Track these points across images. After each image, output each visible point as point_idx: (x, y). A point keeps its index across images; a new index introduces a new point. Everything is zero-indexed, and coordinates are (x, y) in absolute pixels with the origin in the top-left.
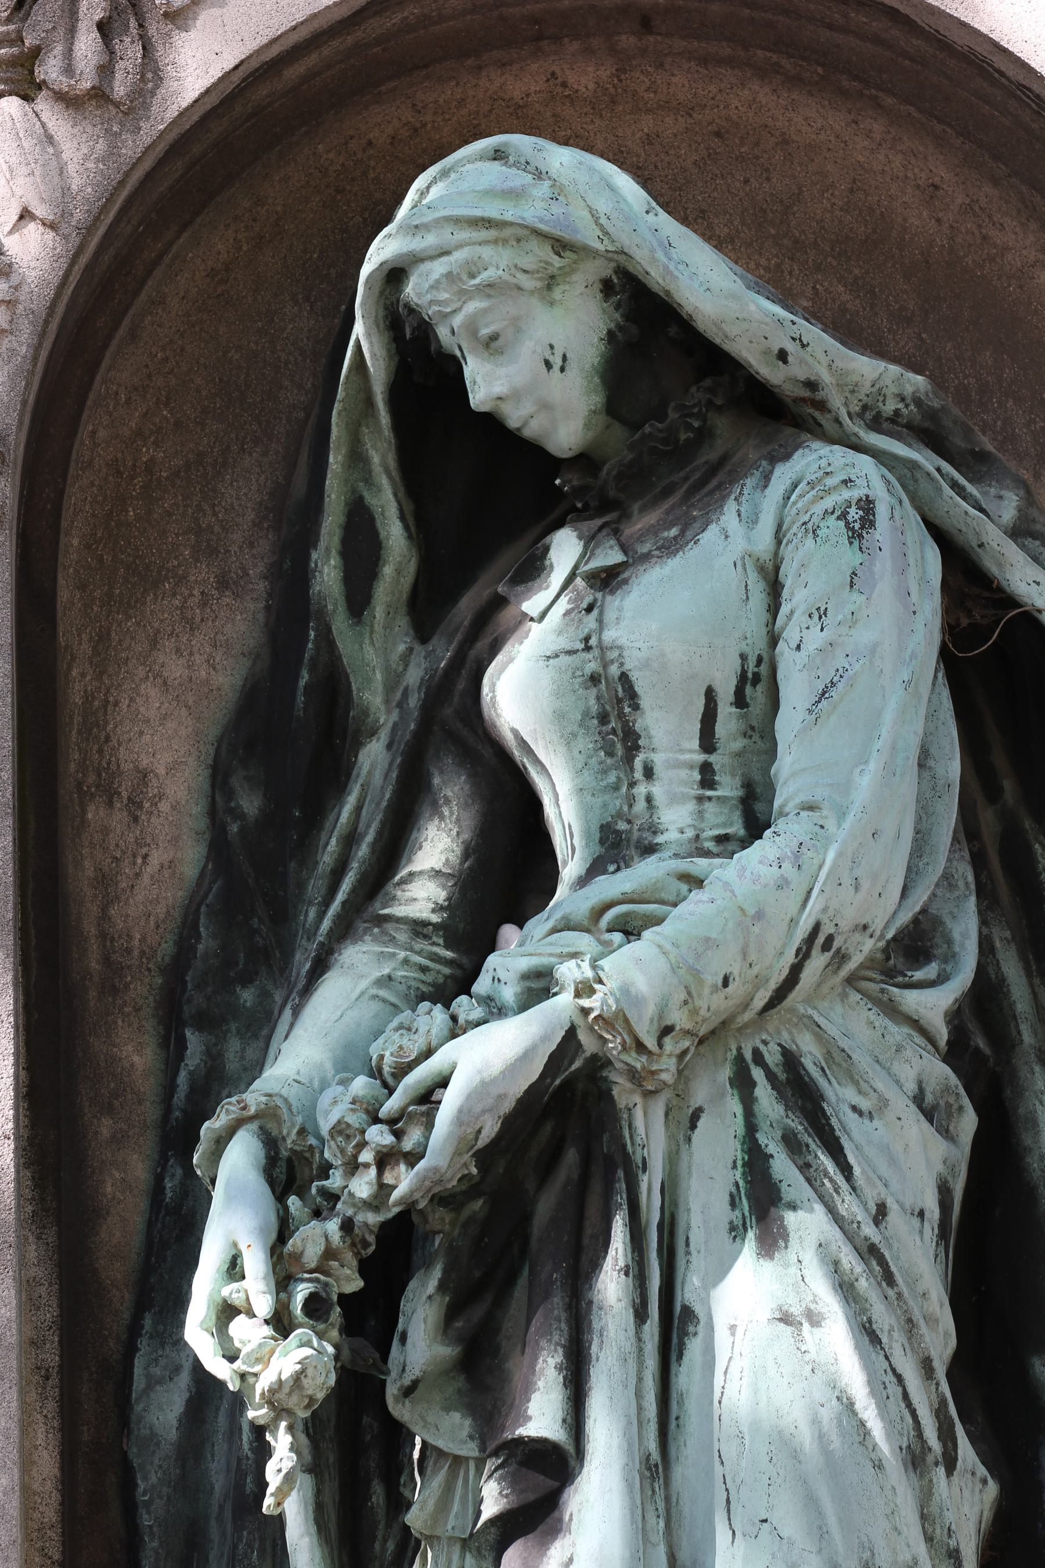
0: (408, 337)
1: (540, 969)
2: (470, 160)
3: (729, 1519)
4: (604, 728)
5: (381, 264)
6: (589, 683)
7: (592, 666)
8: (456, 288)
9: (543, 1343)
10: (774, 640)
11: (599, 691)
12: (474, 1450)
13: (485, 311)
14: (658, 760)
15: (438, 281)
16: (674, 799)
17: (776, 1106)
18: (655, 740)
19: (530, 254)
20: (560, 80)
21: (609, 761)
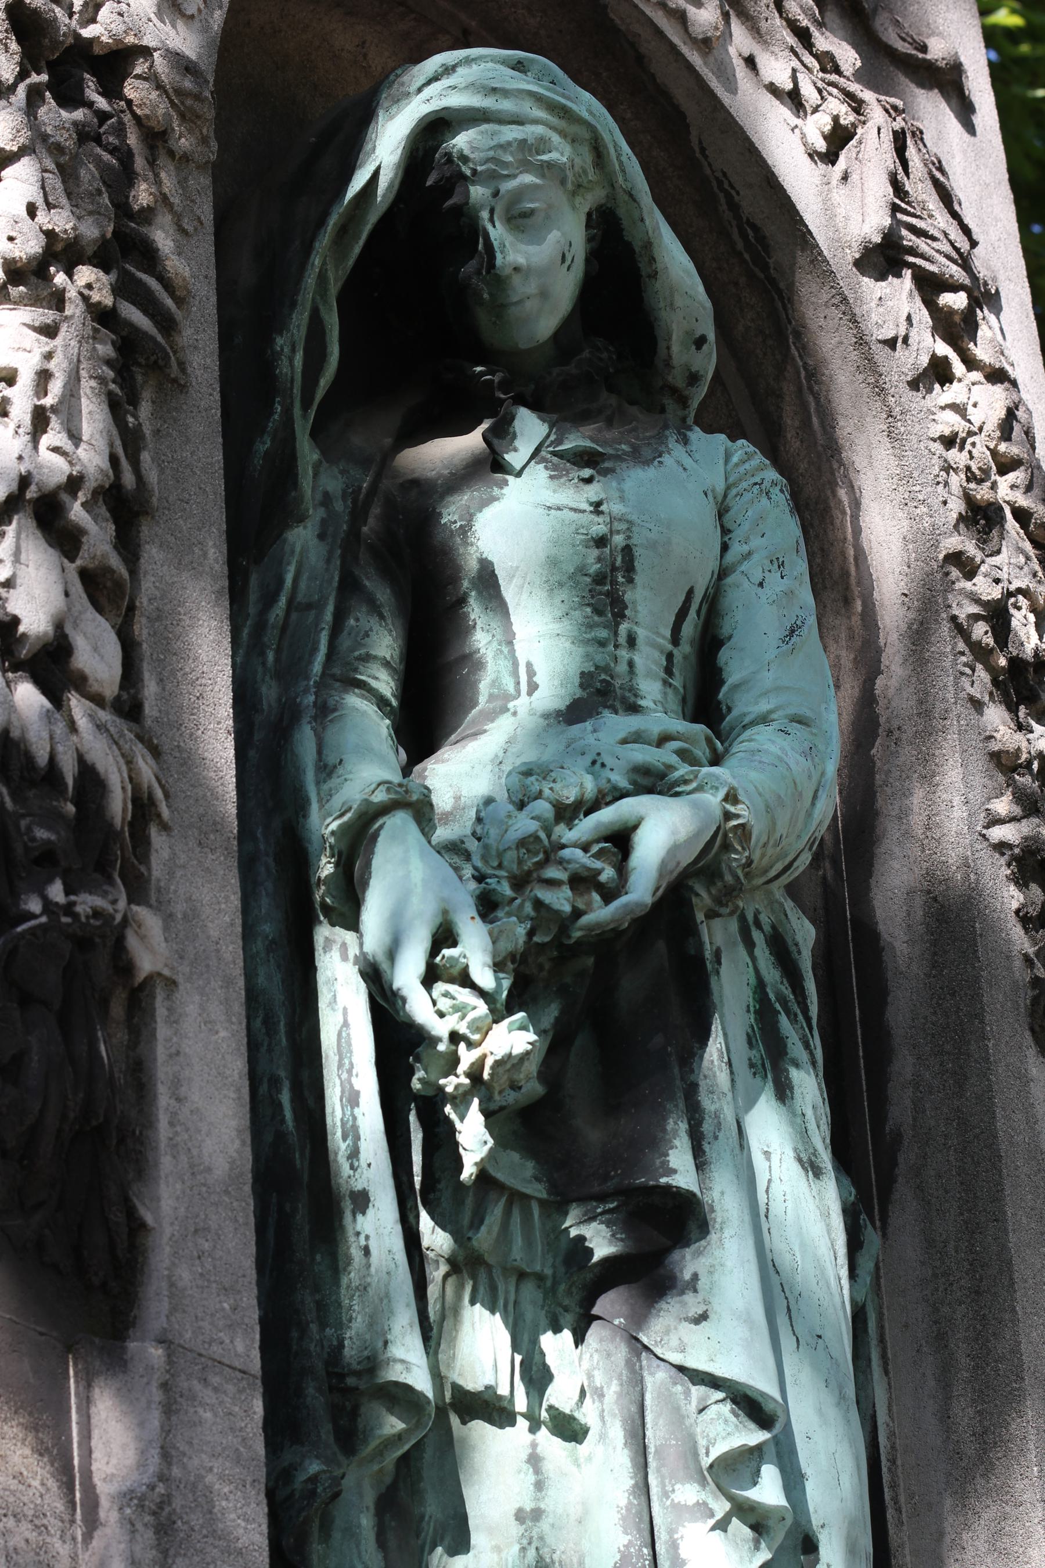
0: (429, 183)
3: (792, 1325)
6: (592, 543)
8: (521, 157)
9: (669, 1106)
10: (723, 573)
12: (540, 1191)
13: (534, 187)
14: (641, 633)
15: (509, 143)
16: (649, 674)
17: (772, 970)
18: (640, 615)
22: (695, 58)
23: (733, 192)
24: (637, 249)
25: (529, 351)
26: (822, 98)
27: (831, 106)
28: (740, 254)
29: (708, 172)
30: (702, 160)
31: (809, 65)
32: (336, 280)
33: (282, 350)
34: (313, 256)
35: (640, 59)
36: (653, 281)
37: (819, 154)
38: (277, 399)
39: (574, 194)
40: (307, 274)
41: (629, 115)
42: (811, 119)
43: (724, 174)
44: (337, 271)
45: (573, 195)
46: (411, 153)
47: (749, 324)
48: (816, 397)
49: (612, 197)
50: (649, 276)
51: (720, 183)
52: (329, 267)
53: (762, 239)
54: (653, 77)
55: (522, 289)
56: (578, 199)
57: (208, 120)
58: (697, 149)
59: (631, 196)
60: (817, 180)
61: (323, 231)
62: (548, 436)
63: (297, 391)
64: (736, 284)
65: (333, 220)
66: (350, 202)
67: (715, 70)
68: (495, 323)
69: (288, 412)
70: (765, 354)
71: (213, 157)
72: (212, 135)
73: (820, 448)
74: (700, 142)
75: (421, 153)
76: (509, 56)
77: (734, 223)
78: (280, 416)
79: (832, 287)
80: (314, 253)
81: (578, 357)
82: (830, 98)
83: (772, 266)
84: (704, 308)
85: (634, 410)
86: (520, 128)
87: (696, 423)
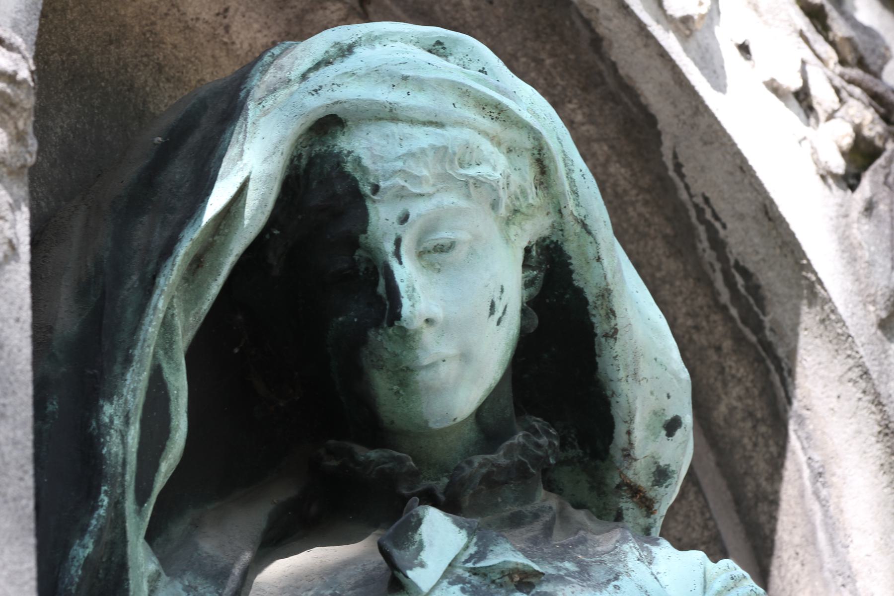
8: (439, 169)
15: (423, 151)
19: (518, 172)
20: (226, 21)
22: (670, 42)
23: (718, 225)
24: (591, 299)
25: (443, 433)
26: (842, 101)
27: (852, 111)
28: (724, 309)
29: (684, 196)
30: (677, 179)
31: (824, 56)
32: (185, 331)
33: (112, 421)
34: (155, 297)
35: (597, 42)
36: (611, 341)
37: (835, 176)
38: (104, 488)
39: (508, 221)
40: (147, 320)
41: (579, 118)
42: (825, 127)
43: (707, 200)
44: (187, 317)
45: (507, 224)
46: (292, 161)
47: (735, 403)
48: (824, 504)
49: (559, 228)
50: (606, 336)
51: (700, 212)
52: (176, 312)
53: (755, 289)
54: (614, 66)
55: (434, 348)
56: (513, 230)
57: (25, 110)
58: (670, 165)
59: (584, 226)
60: (832, 211)
61: (169, 263)
62: (466, 547)
63: (130, 477)
64: (718, 349)
65: (184, 249)
66: (208, 224)
67: (698, 59)
68: (397, 393)
69: (117, 505)
70: (755, 445)
71: (31, 160)
72: (30, 129)
73: (827, 574)
74: (675, 156)
75: (304, 162)
76: (424, 34)
77: (718, 266)
78: (107, 510)
79: (849, 356)
80: (158, 292)
81: (508, 443)
82: (852, 102)
83: (767, 325)
84: (679, 380)
85: (580, 516)
86: (439, 131)
87: (661, 535)
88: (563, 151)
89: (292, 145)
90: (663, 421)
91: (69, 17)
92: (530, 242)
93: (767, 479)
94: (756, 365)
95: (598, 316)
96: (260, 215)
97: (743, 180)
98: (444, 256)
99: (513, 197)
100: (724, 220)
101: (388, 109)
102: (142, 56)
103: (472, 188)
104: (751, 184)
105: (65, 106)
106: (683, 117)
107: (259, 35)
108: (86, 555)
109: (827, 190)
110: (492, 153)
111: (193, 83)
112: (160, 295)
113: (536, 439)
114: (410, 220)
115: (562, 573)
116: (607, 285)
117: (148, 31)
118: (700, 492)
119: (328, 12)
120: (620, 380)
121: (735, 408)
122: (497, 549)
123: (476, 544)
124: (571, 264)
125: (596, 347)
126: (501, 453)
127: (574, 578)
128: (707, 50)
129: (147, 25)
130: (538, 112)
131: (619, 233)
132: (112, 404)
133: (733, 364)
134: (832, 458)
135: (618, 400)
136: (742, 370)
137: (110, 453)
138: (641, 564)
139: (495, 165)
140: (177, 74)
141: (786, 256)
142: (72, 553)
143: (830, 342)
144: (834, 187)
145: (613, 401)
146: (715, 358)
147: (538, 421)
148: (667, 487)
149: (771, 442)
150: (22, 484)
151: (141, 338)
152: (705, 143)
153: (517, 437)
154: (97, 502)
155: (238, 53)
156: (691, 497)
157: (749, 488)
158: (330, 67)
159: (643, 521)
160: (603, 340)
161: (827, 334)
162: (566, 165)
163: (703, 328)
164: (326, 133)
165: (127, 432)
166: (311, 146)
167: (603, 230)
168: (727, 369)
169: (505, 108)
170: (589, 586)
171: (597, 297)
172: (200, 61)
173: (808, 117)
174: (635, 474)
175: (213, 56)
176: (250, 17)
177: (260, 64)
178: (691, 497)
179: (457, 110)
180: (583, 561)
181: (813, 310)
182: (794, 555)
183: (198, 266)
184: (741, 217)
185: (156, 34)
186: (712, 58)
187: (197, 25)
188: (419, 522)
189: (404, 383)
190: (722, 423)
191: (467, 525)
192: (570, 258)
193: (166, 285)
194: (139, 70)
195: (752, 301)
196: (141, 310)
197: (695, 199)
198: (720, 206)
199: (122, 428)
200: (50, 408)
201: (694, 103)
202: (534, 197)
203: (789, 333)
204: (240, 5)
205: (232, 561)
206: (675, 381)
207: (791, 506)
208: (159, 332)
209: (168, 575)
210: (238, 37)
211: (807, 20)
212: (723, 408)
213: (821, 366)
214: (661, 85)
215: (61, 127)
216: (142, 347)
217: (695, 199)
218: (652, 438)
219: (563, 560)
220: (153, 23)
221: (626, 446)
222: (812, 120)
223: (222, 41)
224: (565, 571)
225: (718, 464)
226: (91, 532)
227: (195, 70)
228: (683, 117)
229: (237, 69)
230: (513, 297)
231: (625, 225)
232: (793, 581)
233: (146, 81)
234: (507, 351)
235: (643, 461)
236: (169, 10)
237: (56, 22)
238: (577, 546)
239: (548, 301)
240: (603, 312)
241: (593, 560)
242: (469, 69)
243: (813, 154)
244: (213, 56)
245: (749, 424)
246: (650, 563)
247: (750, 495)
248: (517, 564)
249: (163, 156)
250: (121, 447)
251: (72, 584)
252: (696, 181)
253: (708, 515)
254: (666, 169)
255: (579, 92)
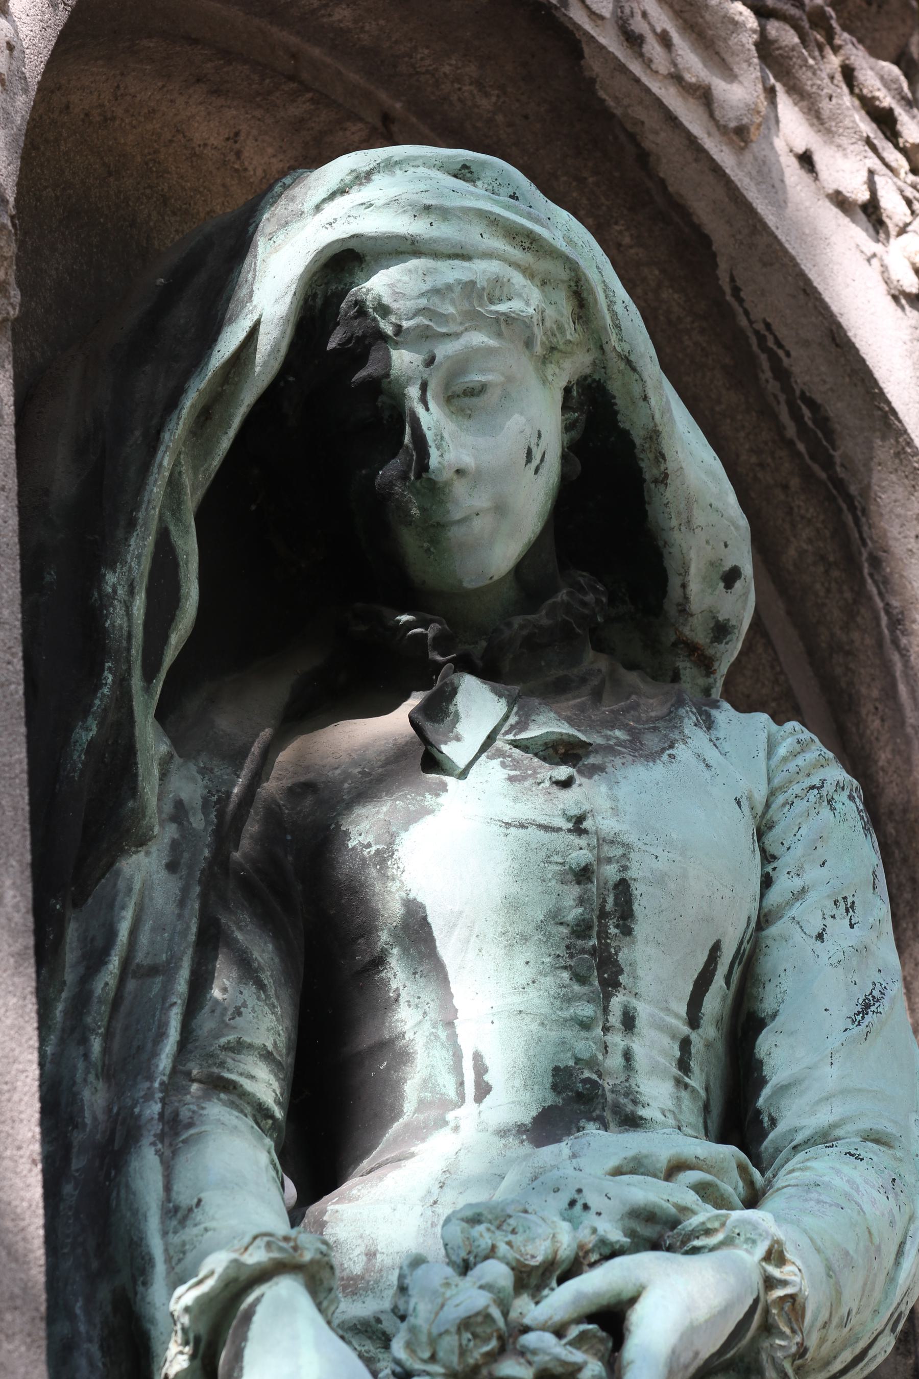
0: (331, 345)
1: (656, 1210)
2: (426, 163)
4: (579, 942)
5: (353, 236)
6: (570, 877)
7: (581, 855)
8: (466, 306)
10: (763, 920)
11: (586, 891)
13: (489, 352)
14: (643, 1011)
15: (449, 287)
19: (554, 306)
21: (576, 988)
23: (781, 353)
24: (638, 441)
25: (479, 592)
28: (791, 444)
29: (743, 322)
30: (735, 305)
32: (194, 489)
33: (115, 591)
34: (160, 454)
35: (643, 158)
36: (662, 487)
38: (108, 665)
39: (545, 360)
40: (151, 479)
43: (768, 326)
44: (195, 474)
45: (544, 363)
46: (306, 301)
47: (805, 546)
49: (601, 364)
50: (656, 481)
51: (761, 339)
52: (183, 469)
53: (823, 421)
54: (662, 184)
55: (467, 500)
56: (551, 369)
57: (6, 258)
58: (727, 289)
59: (629, 362)
62: (506, 718)
63: (136, 652)
64: (785, 487)
65: (190, 400)
69: (123, 683)
70: (828, 591)
71: (14, 313)
72: (12, 280)
74: (732, 279)
75: (319, 302)
76: (449, 157)
77: (782, 398)
80: (162, 448)
81: (550, 601)
83: (838, 460)
84: (737, 528)
85: (632, 678)
86: (466, 264)
88: (604, 282)
89: (306, 284)
90: (721, 572)
91: (63, 148)
92: (569, 382)
93: (841, 628)
94: (827, 503)
95: (646, 460)
96: (272, 361)
97: (807, 304)
98: (474, 400)
99: (549, 333)
100: (787, 348)
101: (409, 242)
102: (145, 188)
103: (503, 326)
104: (815, 307)
105: (59, 246)
106: (739, 237)
107: (274, 160)
108: (89, 738)
109: (899, 310)
110: (525, 286)
111: (202, 215)
112: (165, 452)
113: (581, 596)
114: (436, 363)
115: (611, 743)
116: (656, 425)
117: (151, 160)
118: (769, 644)
119: (348, 133)
120: (672, 529)
121: (806, 551)
122: (541, 718)
123: (516, 713)
124: (616, 404)
125: (645, 493)
126: (544, 612)
127: (625, 747)
128: (764, 162)
129: (149, 154)
130: (576, 239)
131: (666, 367)
132: (115, 572)
133: (802, 504)
134: (912, 603)
135: (671, 550)
136: (811, 510)
137: (114, 626)
138: (699, 730)
139: (526, 300)
140: (184, 206)
141: (855, 385)
142: (75, 736)
143: (907, 477)
144: (907, 307)
145: (665, 552)
146: (782, 497)
147: (583, 576)
148: (727, 643)
149: (845, 588)
150: (10, 667)
151: (146, 499)
152: (765, 265)
153: (560, 594)
154: (101, 680)
155: (251, 180)
156: (760, 650)
157: (823, 637)
158: (346, 197)
159: (702, 681)
160: (653, 486)
161: (903, 468)
162: (607, 297)
163: (768, 465)
164: (342, 270)
165: (131, 603)
166: (326, 284)
167: (649, 366)
168: (796, 510)
169: (537, 237)
170: (641, 756)
171: (644, 439)
172: (209, 191)
173: (877, 233)
174: (692, 630)
175: (224, 185)
176: (263, 141)
177: (270, 195)
178: (760, 650)
179: (485, 240)
180: (635, 728)
181: (887, 443)
182: (873, 710)
183: (207, 419)
184: (806, 344)
185: (159, 163)
186: (770, 171)
187: (205, 152)
188: (454, 692)
189: (435, 541)
190: (791, 568)
191: (507, 693)
192: (614, 397)
193: (171, 441)
194: (142, 203)
195: (820, 435)
196: (145, 468)
197: (755, 326)
198: (782, 332)
199: (126, 598)
200: (48, 578)
201: (750, 221)
202: (571, 333)
203: (862, 469)
204: (252, 128)
205: (251, 740)
206: (732, 528)
207: (868, 657)
208: (165, 492)
209: (180, 756)
210: (251, 164)
211: (874, 126)
212: (792, 552)
213: (897, 504)
214: (714, 202)
215: (57, 269)
216: (146, 509)
217: (755, 326)
218: (710, 591)
219: (613, 728)
220: (156, 152)
221: (681, 600)
222: (882, 236)
223: (232, 167)
224: (615, 741)
225: (789, 613)
226: (94, 713)
227: (204, 201)
228: (739, 237)
229: (250, 197)
230: (552, 444)
231: (680, 355)
232: (873, 738)
233: (150, 215)
234: (546, 502)
235: (699, 616)
236: (174, 136)
237: (48, 154)
238: (628, 712)
239: (591, 444)
240: (651, 456)
241: (646, 726)
242: (498, 195)
243: (883, 272)
244: (224, 185)
245: (821, 569)
246: (709, 728)
247: (824, 645)
248: (561, 734)
249: (167, 298)
250: (125, 619)
251: (74, 771)
252: (756, 306)
253: (778, 669)
254: (723, 293)
255: (625, 212)
